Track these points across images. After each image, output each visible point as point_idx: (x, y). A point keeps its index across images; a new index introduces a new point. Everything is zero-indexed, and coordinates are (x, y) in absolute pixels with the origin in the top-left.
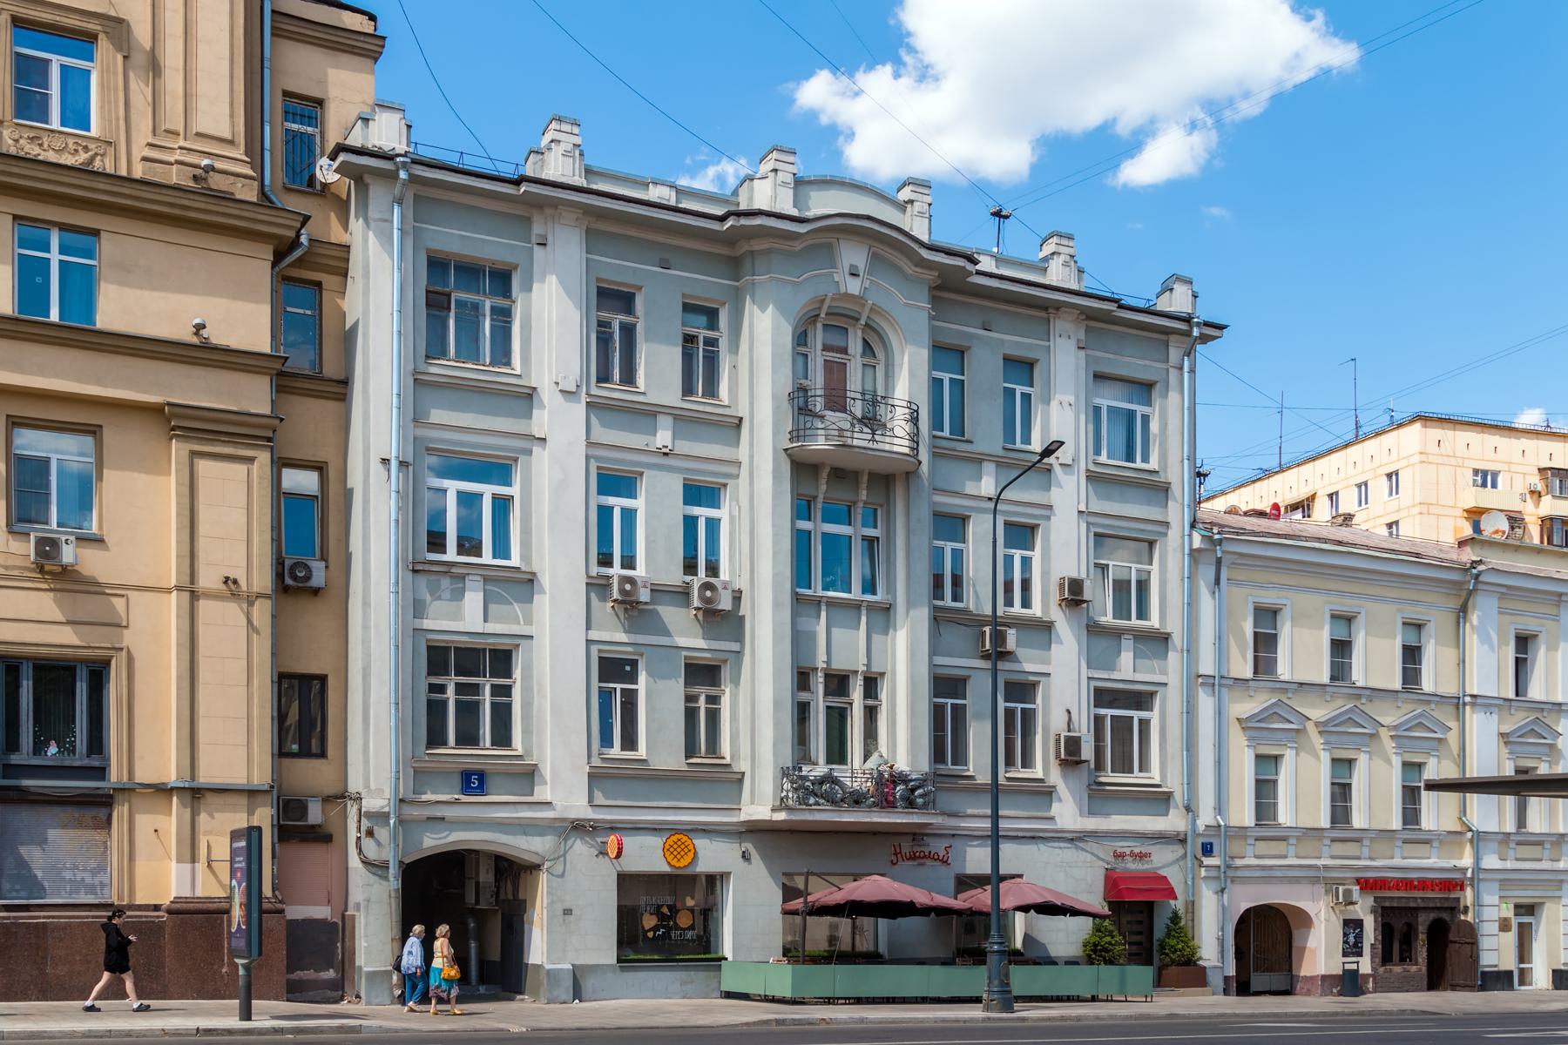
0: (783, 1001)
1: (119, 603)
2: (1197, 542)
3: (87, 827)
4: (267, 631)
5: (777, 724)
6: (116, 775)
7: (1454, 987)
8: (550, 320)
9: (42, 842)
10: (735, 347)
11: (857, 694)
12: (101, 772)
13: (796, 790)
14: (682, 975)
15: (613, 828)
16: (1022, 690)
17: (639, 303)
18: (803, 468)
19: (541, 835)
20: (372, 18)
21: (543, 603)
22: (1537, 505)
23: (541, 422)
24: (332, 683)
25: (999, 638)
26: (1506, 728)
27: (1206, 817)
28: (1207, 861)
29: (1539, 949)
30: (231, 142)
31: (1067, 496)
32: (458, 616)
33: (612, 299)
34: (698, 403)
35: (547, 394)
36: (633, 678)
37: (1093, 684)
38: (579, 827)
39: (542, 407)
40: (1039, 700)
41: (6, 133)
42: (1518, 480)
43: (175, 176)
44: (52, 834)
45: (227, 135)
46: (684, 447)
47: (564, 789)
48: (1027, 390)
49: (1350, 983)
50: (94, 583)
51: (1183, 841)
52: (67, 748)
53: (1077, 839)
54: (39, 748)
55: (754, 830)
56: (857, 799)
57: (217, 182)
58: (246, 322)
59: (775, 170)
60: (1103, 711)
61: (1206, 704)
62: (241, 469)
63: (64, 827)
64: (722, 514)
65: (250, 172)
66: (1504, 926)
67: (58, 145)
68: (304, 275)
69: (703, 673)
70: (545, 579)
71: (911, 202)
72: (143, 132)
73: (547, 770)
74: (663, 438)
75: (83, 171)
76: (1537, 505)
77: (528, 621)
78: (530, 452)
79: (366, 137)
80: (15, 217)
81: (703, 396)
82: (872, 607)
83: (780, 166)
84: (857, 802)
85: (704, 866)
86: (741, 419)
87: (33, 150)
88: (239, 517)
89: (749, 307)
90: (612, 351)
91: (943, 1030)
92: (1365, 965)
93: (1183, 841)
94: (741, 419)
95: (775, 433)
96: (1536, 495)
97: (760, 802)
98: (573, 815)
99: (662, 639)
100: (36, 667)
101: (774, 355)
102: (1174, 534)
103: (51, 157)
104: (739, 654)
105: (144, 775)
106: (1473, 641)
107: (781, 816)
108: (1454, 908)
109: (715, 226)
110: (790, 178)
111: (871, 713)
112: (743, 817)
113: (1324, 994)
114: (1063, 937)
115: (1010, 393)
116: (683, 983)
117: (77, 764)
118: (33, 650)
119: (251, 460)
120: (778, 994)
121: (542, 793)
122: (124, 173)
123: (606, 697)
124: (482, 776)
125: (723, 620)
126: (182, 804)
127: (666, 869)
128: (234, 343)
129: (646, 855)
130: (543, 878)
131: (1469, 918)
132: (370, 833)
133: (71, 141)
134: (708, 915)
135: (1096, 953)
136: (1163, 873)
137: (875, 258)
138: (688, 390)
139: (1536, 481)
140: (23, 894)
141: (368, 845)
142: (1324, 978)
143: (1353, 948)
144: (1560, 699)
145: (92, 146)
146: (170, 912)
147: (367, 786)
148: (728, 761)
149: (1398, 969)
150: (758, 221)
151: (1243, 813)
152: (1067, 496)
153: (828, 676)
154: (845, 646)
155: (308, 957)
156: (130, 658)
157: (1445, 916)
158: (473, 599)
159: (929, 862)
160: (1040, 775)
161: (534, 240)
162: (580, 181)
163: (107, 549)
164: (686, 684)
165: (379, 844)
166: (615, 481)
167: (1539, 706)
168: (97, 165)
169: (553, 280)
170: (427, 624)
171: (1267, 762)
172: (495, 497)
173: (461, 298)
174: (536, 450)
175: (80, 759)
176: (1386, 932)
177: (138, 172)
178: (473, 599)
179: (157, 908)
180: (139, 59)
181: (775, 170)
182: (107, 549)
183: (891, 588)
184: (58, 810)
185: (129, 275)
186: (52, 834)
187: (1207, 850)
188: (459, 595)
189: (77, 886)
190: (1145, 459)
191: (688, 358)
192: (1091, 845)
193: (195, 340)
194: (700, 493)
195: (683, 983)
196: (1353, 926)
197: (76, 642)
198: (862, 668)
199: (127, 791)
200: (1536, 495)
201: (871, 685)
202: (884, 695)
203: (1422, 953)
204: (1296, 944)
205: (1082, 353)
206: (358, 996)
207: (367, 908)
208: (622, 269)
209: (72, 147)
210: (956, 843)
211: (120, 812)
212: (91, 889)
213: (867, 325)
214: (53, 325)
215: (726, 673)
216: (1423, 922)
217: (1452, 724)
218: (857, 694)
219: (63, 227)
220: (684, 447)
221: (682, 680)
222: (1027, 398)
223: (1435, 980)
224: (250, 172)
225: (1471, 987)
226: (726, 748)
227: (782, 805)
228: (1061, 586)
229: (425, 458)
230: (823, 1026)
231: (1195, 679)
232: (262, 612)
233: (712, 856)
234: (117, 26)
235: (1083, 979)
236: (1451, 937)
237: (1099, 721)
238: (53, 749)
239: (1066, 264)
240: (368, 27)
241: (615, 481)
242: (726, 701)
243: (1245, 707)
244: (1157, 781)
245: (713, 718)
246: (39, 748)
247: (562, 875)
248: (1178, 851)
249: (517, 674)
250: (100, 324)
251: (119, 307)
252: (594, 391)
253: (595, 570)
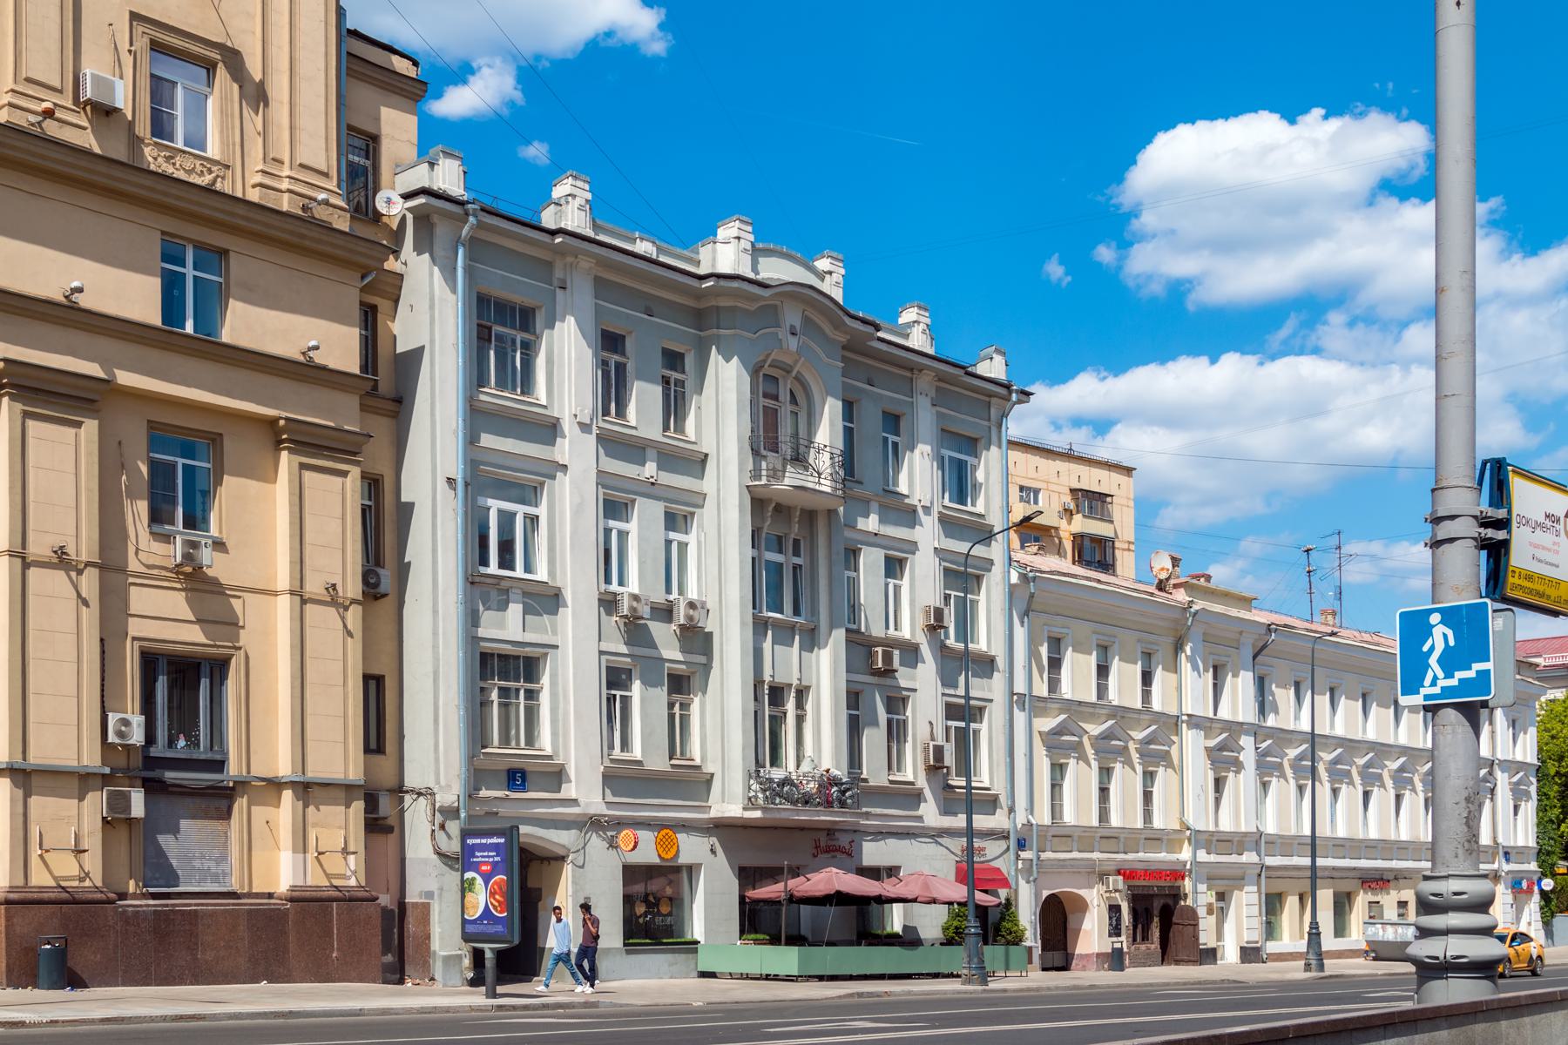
0: (789, 979)
1: (236, 604)
2: (1014, 578)
3: (211, 818)
4: (358, 634)
5: (836, 736)
6: (234, 769)
7: (1177, 962)
8: (565, 361)
9: (175, 831)
10: (699, 389)
11: (790, 706)
12: (219, 765)
13: (764, 791)
14: (669, 957)
15: (619, 824)
16: (896, 702)
17: (629, 344)
18: (760, 504)
19: (568, 829)
20: (415, 64)
21: (567, 615)
22: (1069, 523)
23: (563, 450)
24: (389, 684)
25: (888, 657)
26: (1212, 743)
27: (1021, 818)
28: (1023, 855)
29: (1229, 927)
30: (60, 92)
31: (927, 534)
32: (501, 625)
33: (610, 342)
34: (671, 439)
35: (567, 425)
36: (627, 687)
37: (604, 658)
38: (594, 823)
39: (564, 437)
40: (909, 713)
41: (147, 150)
42: (1055, 497)
43: (285, 203)
44: (184, 823)
45: (57, 85)
46: (667, 478)
47: (585, 791)
48: (896, 439)
49: (1115, 960)
50: (215, 582)
51: (1007, 838)
52: (194, 742)
53: (937, 834)
54: (171, 743)
55: (724, 829)
56: (807, 800)
57: (321, 213)
58: (339, 347)
59: (738, 238)
60: (950, 723)
61: (1020, 717)
62: (337, 481)
63: (194, 817)
64: (542, 511)
65: (343, 204)
66: (1210, 912)
67: (188, 166)
68: (374, 304)
69: (680, 684)
70: (568, 595)
71: (830, 273)
72: (256, 162)
73: (572, 771)
74: (650, 469)
75: (209, 190)
76: (1069, 523)
77: (555, 633)
78: (553, 477)
79: (431, 179)
80: (163, 233)
82: (777, 625)
83: (743, 234)
84: (807, 803)
85: (683, 859)
86: (706, 455)
87: (170, 170)
88: (336, 526)
89: (715, 356)
90: (613, 389)
91: (958, 1000)
92: (1123, 941)
93: (1007, 838)
94: (706, 455)
95: (741, 470)
96: (1068, 513)
97: (730, 800)
98: (592, 811)
99: (655, 655)
100: (170, 663)
101: (739, 401)
102: (997, 570)
103: (181, 175)
104: (707, 667)
105: (259, 770)
106: (1186, 666)
107: (758, 814)
108: (1177, 895)
109: (694, 283)
110: (749, 247)
111: (800, 720)
112: (713, 814)
113: (1098, 970)
114: (931, 922)
115: (886, 440)
116: (671, 965)
117: (203, 757)
118: (171, 647)
119: (78, 425)
120: (782, 972)
121: (569, 791)
122: (239, 194)
123: (611, 700)
124: (523, 773)
125: (697, 639)
126: (297, 797)
127: (657, 861)
128: (897, 949)
129: (647, 851)
130: (568, 870)
131: (1189, 902)
132: (442, 827)
133: (198, 163)
134: (678, 903)
135: (953, 938)
136: (995, 864)
137: (807, 321)
138: (666, 428)
139: (1067, 499)
140: (162, 882)
141: (440, 835)
142: (1098, 955)
143: (1115, 931)
144: (1241, 720)
145: (214, 168)
146: (292, 900)
147: (438, 782)
148: (698, 762)
149: (1143, 947)
150: (735, 284)
151: (1043, 817)
152: (927, 534)
153: (772, 689)
154: (785, 662)
155: (392, 942)
156: (247, 657)
157: (1170, 902)
158: (515, 610)
159: (839, 855)
160: (910, 778)
161: (556, 283)
162: (590, 233)
163: (227, 552)
164: (670, 694)
165: (449, 837)
166: (614, 508)
167: (1160, 717)
168: (218, 186)
169: (570, 320)
170: (482, 632)
171: (1058, 770)
172: (526, 516)
173: (501, 331)
174: (559, 474)
175: (202, 753)
176: (1135, 912)
177: (254, 195)
178: (515, 610)
179: (270, 896)
180: (250, 89)
181: (738, 238)
182: (227, 552)
183: (814, 611)
184: (188, 801)
186: (184, 823)
187: (1021, 845)
188: (503, 606)
189: (205, 875)
190: (973, 504)
191: (666, 396)
192: (945, 841)
193: (302, 359)
194: (675, 521)
195: (671, 965)
196: (1114, 909)
197: (204, 640)
198: (795, 682)
199: (241, 786)
200: (1068, 513)
201: (801, 694)
202: (809, 707)
203: (1156, 933)
204: (1071, 924)
205: (934, 410)
206: (432, 979)
207: (440, 895)
208: (623, 317)
209: (198, 168)
210: (856, 837)
211: (240, 804)
212: (216, 878)
213: (796, 378)
214: (187, 336)
215: (696, 682)
216: (1157, 905)
217: (1174, 738)
218: (790, 706)
219: (198, 246)
220: (667, 478)
221: (665, 688)
222: (895, 445)
223: (1166, 954)
224: (343, 204)
225: (1194, 962)
226: (545, 742)
227: (751, 803)
228: (927, 613)
229: (479, 479)
230: (886, 998)
231: (1017, 700)
232: (354, 616)
233: (692, 848)
234: (233, 59)
235: (957, 958)
236: (1175, 920)
237: (948, 729)
238: (182, 743)
239: (924, 332)
240: (411, 71)
241: (614, 508)
242: (545, 699)
243: (1046, 724)
244: (986, 785)
245: (685, 720)
246: (171, 743)
247: (582, 867)
248: (1002, 845)
249: (545, 680)
250: (226, 336)
251: (246, 324)
252: (602, 424)
253: (603, 587)
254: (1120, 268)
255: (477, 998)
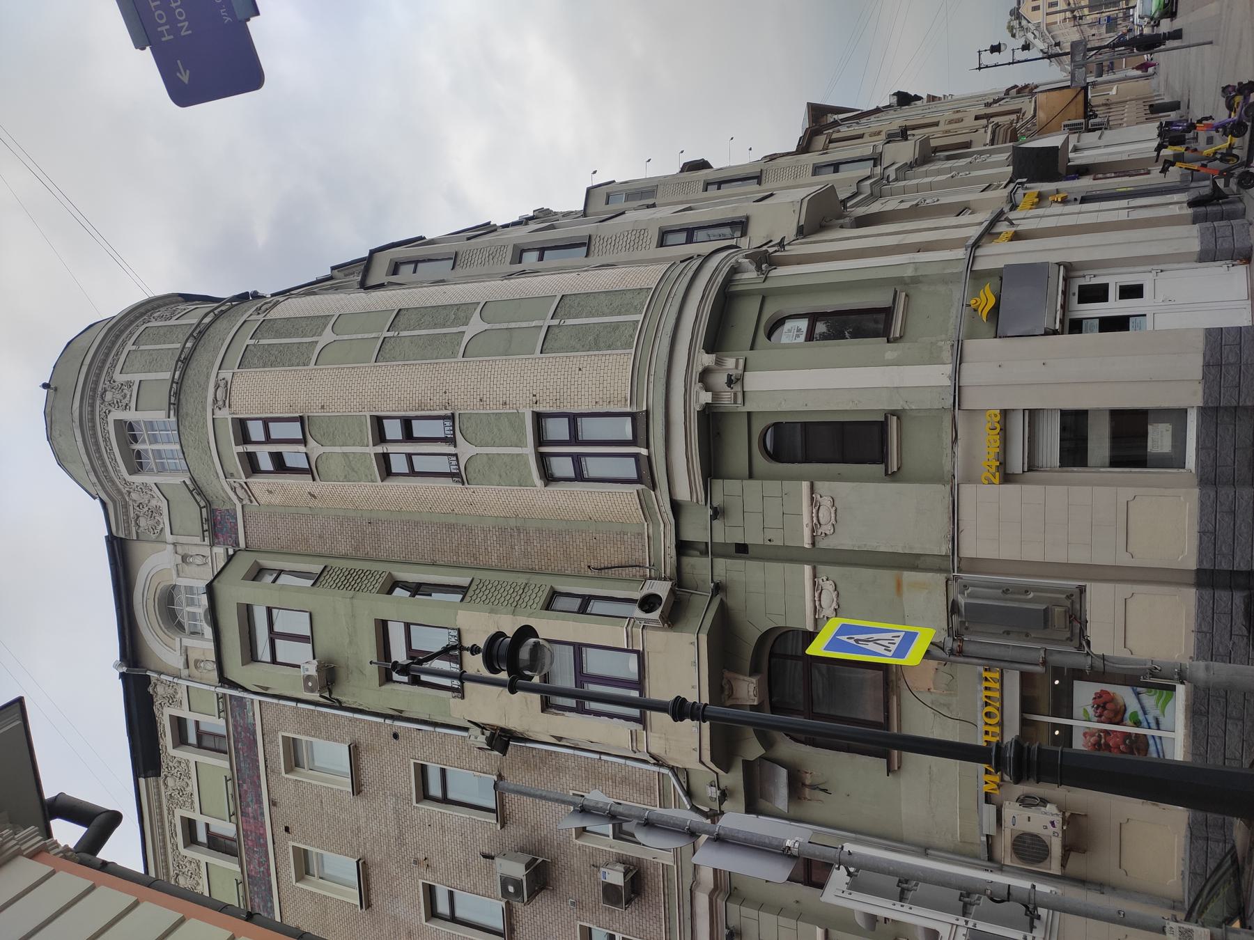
81: (1106, 286)
254: (886, 724)
255: (1247, 136)
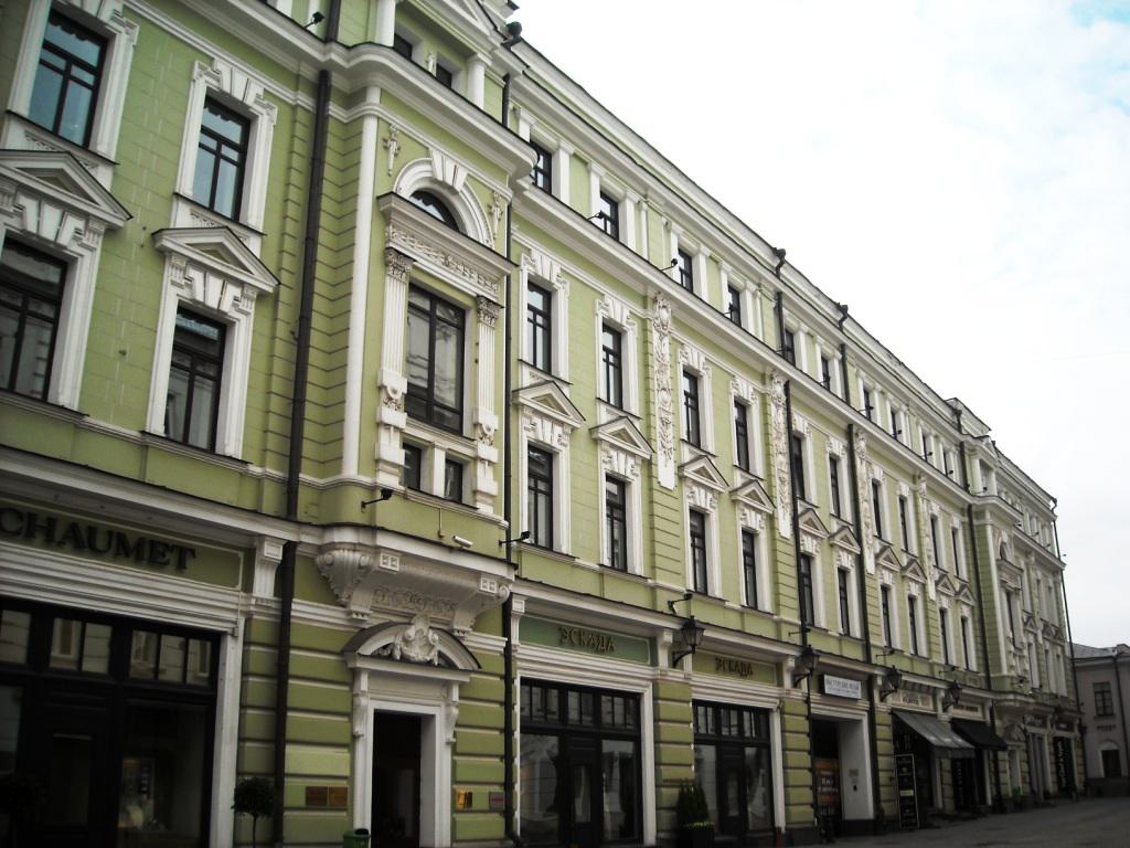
45: (207, 205)
185: (763, 605)
